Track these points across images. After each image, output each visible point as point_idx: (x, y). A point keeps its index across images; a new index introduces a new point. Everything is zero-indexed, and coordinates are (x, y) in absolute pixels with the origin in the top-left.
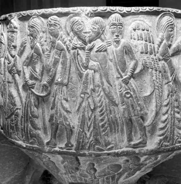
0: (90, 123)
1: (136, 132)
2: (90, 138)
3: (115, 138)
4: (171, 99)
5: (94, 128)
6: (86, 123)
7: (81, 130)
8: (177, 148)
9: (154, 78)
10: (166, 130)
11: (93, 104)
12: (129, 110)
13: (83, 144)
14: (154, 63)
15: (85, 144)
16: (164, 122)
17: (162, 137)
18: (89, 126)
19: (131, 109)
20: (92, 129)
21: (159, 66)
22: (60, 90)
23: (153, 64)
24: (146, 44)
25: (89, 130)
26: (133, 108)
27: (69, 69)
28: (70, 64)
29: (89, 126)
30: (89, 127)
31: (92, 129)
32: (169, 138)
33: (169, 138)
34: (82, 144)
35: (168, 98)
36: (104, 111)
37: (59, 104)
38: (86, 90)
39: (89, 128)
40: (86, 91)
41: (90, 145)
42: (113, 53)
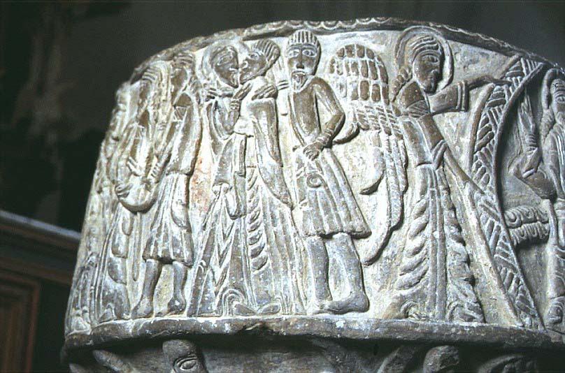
0: (226, 246)
1: (338, 279)
2: (222, 281)
3: (285, 287)
4: (432, 202)
5: (233, 257)
6: (216, 248)
7: (204, 264)
8: (457, 331)
9: (384, 149)
10: (419, 273)
11: (236, 204)
12: (318, 215)
13: (206, 299)
14: (382, 118)
15: (211, 300)
16: (416, 252)
17: (406, 292)
18: (221, 253)
19: (322, 212)
20: (228, 259)
21: (396, 124)
22: (174, 184)
23: (388, 121)
24: (365, 81)
25: (221, 263)
26: (327, 211)
27: (196, 140)
28: (293, 218)
29: (221, 253)
30: (223, 255)
31: (228, 259)
32: (429, 297)
33: (429, 297)
34: (203, 297)
35: (422, 198)
36: (258, 220)
37: (167, 212)
38: (223, 176)
39: (222, 258)
40: (222, 178)
41: (221, 299)
42: (289, 99)
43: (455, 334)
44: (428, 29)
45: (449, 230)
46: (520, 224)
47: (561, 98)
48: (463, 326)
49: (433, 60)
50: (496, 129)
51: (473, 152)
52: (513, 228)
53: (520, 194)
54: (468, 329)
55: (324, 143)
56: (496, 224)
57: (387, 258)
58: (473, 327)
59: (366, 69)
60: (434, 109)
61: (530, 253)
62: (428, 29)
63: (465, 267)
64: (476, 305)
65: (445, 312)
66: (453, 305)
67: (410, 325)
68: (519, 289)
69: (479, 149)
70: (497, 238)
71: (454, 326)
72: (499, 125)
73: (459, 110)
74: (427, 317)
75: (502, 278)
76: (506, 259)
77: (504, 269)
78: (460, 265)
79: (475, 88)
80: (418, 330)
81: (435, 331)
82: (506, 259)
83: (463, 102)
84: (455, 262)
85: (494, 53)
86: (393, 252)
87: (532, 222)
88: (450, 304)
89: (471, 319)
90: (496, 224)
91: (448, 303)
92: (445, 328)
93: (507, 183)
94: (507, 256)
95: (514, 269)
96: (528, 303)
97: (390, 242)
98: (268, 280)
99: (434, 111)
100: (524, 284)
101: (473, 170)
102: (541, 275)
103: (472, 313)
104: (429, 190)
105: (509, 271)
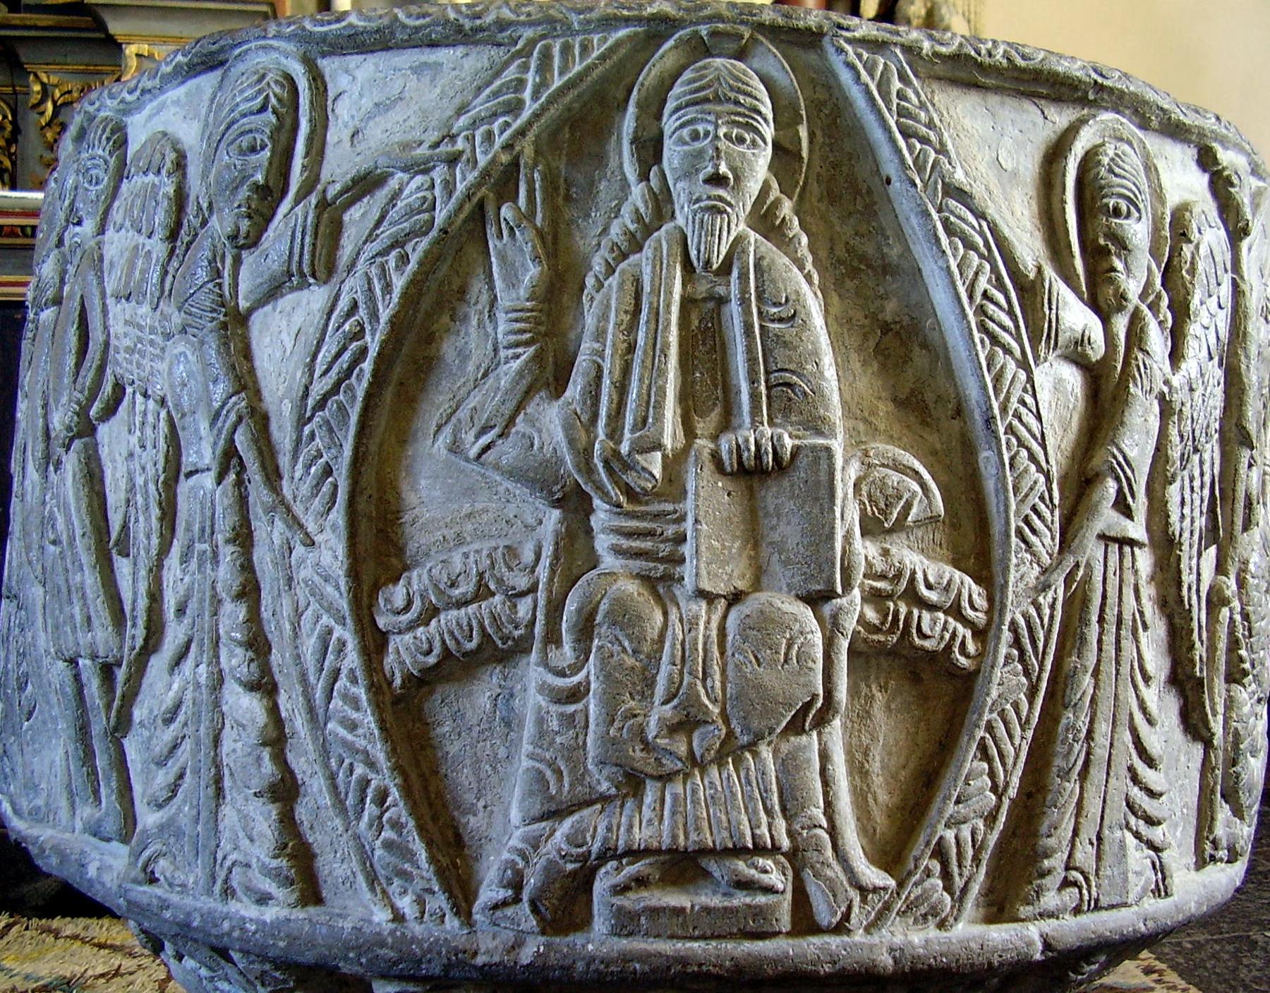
3: (52, 763)
43: (229, 934)
44: (263, 48)
45: (235, 660)
46: (431, 613)
47: (685, 132)
48: (243, 919)
49: (253, 150)
50: (373, 335)
51: (302, 421)
52: (400, 633)
53: (467, 508)
54: (254, 928)
55: (69, 429)
56: (338, 632)
57: (141, 724)
58: (264, 923)
59: (259, 166)
60: (246, 299)
61: (471, 693)
62: (263, 48)
63: (259, 758)
64: (274, 863)
65: (213, 879)
66: (228, 863)
67: (155, 901)
68: (384, 819)
69: (321, 404)
70: (336, 674)
71: (226, 917)
72: (385, 315)
73: (303, 285)
74: (183, 886)
75: (342, 788)
76: (350, 737)
77: (347, 761)
78: (250, 754)
79: (364, 196)
80: (167, 914)
81: (195, 924)
82: (350, 737)
83: (306, 256)
84: (239, 744)
85: (460, 50)
86: (151, 711)
87: (467, 603)
88: (225, 858)
89: (263, 899)
90: (338, 632)
91: (220, 856)
92: (209, 916)
93: (423, 482)
94: (353, 726)
95: (371, 764)
96: (409, 855)
97: (144, 686)
98: (37, 746)
99: (248, 305)
100: (401, 804)
101: (298, 475)
102: (502, 753)
103: (269, 886)
104: (199, 547)
105: (360, 770)
